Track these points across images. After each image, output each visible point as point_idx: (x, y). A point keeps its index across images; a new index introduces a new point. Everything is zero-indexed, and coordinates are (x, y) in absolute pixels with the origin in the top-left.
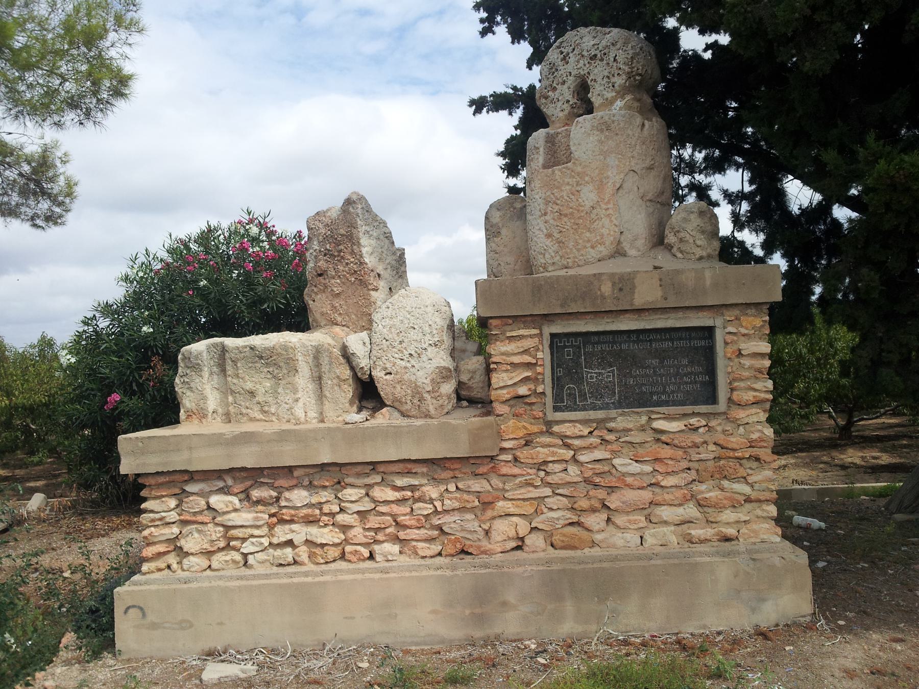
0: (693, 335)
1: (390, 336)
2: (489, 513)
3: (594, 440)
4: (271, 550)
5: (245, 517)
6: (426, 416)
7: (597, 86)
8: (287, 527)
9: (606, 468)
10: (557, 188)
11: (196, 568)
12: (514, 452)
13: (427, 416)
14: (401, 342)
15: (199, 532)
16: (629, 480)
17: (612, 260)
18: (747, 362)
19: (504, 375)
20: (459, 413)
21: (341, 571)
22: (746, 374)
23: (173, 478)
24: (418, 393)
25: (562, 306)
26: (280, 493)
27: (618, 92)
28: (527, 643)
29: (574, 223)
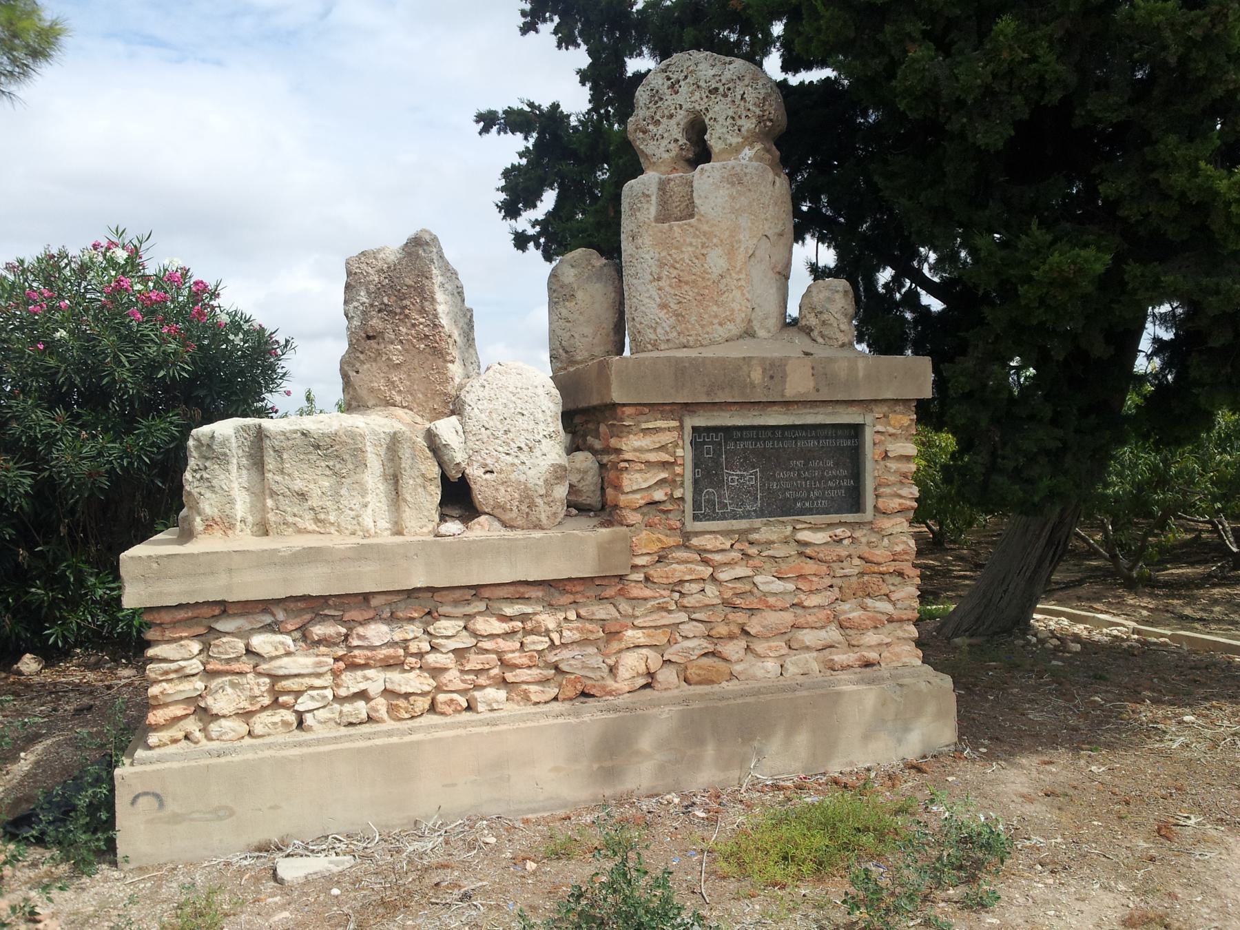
0: (840, 432)
1: (491, 423)
2: (615, 646)
3: (735, 555)
4: (336, 706)
5: (302, 662)
6: (535, 527)
7: (717, 127)
8: (359, 673)
9: (748, 588)
10: (677, 248)
11: (232, 735)
12: (646, 570)
13: (538, 526)
14: (506, 432)
15: (234, 685)
16: (771, 600)
17: (741, 341)
18: (893, 466)
19: (637, 475)
20: (570, 523)
21: (435, 726)
22: (892, 478)
23: (196, 612)
24: (528, 497)
25: (708, 394)
26: (350, 629)
27: (746, 138)
28: (668, 797)
29: (698, 294)
